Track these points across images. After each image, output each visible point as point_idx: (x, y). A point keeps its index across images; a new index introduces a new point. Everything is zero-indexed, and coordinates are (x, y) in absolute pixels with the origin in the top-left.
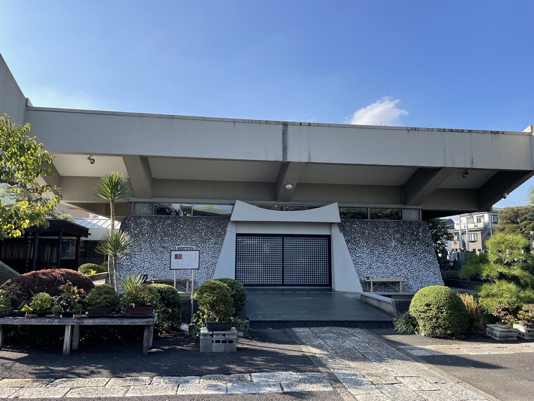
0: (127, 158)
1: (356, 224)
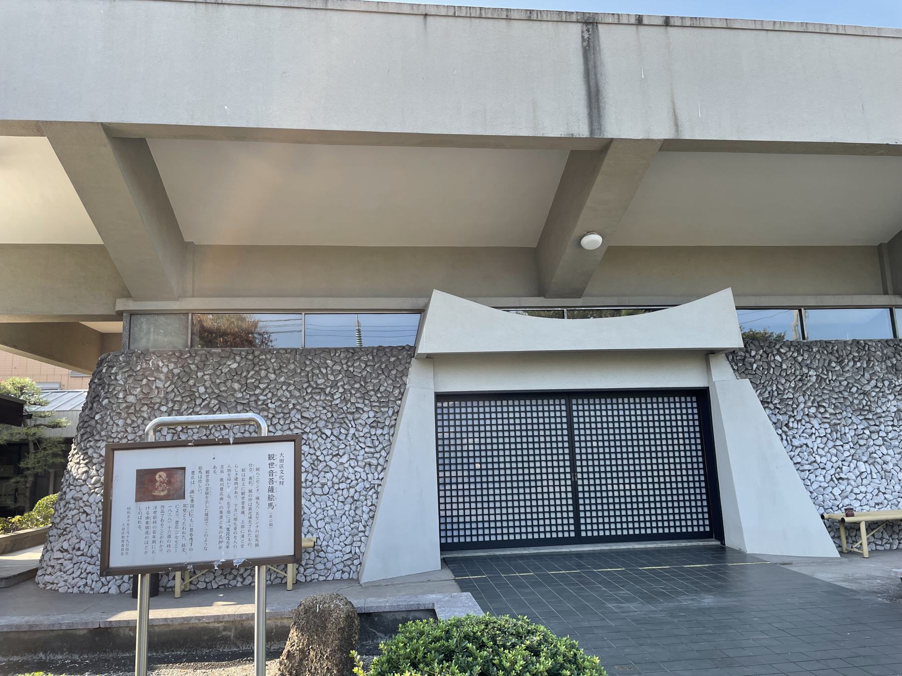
0: (65, 137)
1: (779, 353)
